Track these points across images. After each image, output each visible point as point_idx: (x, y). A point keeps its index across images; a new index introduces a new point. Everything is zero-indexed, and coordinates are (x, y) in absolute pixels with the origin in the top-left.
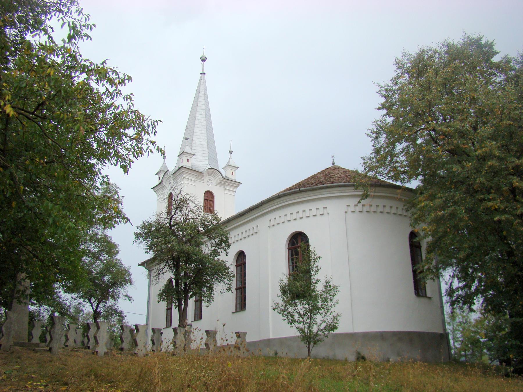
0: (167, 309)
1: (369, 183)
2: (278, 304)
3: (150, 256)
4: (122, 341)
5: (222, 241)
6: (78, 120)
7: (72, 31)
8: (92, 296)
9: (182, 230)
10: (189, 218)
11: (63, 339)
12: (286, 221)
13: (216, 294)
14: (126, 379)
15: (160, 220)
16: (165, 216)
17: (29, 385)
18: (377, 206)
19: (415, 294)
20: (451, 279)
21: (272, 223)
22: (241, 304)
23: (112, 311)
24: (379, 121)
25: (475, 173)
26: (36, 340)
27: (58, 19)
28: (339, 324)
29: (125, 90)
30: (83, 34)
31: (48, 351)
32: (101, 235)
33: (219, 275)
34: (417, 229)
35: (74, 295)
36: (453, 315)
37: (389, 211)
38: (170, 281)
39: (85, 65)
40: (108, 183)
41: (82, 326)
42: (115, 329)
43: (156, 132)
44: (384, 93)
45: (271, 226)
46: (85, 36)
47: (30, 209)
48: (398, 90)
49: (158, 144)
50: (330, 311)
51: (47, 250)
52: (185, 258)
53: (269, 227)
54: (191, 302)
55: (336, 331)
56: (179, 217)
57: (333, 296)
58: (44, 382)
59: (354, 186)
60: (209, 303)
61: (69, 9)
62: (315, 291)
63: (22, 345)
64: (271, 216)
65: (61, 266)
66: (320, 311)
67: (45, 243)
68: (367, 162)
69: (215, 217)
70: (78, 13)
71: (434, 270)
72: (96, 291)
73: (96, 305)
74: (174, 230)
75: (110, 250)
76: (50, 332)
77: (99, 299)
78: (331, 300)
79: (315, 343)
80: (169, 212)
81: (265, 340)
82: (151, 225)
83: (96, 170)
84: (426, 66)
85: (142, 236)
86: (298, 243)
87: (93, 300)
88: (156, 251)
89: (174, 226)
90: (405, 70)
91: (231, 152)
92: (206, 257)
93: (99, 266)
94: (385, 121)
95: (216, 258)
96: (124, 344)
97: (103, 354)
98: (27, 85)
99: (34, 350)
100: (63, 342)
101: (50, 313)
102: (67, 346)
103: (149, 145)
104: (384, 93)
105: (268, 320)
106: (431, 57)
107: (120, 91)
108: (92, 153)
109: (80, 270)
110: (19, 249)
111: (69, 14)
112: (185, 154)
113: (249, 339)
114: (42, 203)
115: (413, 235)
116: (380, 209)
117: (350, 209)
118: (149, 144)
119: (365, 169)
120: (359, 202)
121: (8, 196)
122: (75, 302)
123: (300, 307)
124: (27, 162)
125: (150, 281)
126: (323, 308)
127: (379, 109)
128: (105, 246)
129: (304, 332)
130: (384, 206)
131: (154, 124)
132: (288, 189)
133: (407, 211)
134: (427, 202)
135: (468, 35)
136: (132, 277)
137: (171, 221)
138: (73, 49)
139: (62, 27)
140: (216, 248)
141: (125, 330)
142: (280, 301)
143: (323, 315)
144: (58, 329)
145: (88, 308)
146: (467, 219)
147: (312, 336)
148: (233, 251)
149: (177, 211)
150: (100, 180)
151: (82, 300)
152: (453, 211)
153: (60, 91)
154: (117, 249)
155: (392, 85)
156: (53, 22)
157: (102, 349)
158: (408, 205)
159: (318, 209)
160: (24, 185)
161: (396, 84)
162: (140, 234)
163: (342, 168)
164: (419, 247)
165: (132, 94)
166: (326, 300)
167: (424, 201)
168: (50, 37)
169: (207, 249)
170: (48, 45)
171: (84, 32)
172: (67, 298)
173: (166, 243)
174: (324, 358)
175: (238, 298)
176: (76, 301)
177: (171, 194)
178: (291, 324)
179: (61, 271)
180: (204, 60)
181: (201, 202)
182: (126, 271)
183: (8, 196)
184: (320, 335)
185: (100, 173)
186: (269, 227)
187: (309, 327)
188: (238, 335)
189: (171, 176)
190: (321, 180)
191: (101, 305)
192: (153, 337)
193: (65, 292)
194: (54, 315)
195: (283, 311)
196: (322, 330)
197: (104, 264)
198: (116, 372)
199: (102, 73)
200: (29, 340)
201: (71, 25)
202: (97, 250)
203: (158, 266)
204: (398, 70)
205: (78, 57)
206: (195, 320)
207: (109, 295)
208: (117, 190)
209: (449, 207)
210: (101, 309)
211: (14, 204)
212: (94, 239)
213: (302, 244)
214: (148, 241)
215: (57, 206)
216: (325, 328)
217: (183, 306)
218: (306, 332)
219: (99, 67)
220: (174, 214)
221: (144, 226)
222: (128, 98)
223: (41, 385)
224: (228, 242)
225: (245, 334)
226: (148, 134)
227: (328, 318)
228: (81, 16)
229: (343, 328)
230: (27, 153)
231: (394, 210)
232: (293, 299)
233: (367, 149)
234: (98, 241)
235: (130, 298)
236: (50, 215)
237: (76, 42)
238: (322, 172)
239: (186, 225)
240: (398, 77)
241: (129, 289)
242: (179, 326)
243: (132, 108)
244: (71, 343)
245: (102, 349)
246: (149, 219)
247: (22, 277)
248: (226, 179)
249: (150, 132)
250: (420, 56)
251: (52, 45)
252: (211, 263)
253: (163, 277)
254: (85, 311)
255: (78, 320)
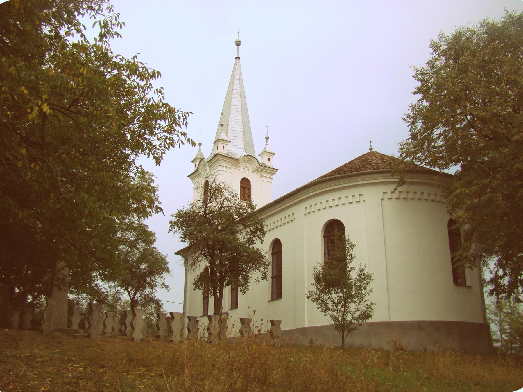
0: (204, 298)
1: (406, 169)
2: (312, 292)
3: (186, 244)
4: (159, 329)
5: (257, 229)
6: (110, 116)
7: (103, 30)
8: (128, 285)
9: (217, 219)
10: (224, 206)
11: (101, 326)
12: (311, 212)
13: (252, 282)
14: (160, 363)
15: (195, 208)
16: (200, 204)
17: (69, 366)
18: (415, 193)
19: (454, 282)
20: (496, 267)
21: (308, 211)
22: (277, 293)
23: (149, 300)
24: (415, 105)
25: (513, 159)
26: (75, 327)
27: (90, 17)
28: (373, 313)
29: (156, 83)
30: (113, 33)
31: (86, 337)
32: (137, 224)
33: (254, 264)
34: (455, 216)
35: (112, 284)
36: (499, 305)
37: (427, 198)
38: (206, 269)
39: (116, 62)
40: (143, 172)
41: (120, 314)
42: (153, 318)
43: (187, 123)
44: (420, 76)
45: (307, 214)
46: (115, 35)
47: (67, 201)
48: (434, 73)
49: (188, 136)
50: (364, 300)
51: (84, 239)
52: (220, 246)
53: (305, 215)
54: (227, 291)
55: (370, 320)
56: (213, 205)
57: (367, 284)
58: (83, 365)
59: (390, 172)
60: (244, 291)
61: (100, 7)
62: (349, 280)
63: (62, 331)
64: (307, 204)
65: (98, 255)
66: (354, 300)
67: (83, 232)
68: (404, 148)
69: (250, 206)
70: (109, 10)
71: (472, 259)
72: (133, 279)
73: (133, 294)
74: (209, 219)
75: (146, 238)
76: (88, 319)
77: (136, 288)
78: (365, 288)
79: (349, 332)
80: (205, 201)
81: (300, 329)
82: (186, 213)
83: (131, 160)
84: (462, 47)
85: (177, 225)
86: (334, 232)
87: (130, 288)
88: (192, 239)
89: (209, 214)
90: (442, 52)
91: (267, 138)
92: (242, 245)
93: (136, 254)
94: (422, 105)
95: (251, 246)
96: (160, 331)
97: (139, 340)
98: (62, 83)
99: (73, 336)
100: (102, 330)
101: (89, 301)
102: (105, 333)
103: (180, 136)
104: (420, 76)
105: (304, 311)
106: (469, 39)
107: (151, 84)
108: (126, 145)
109: (116, 258)
110: (58, 239)
111: (100, 12)
112: (221, 142)
113: (284, 327)
114: (78, 194)
115: (451, 222)
116: (418, 196)
117: (387, 196)
118: (180, 135)
119: (401, 155)
120: (396, 189)
121: (46, 188)
122: (113, 291)
123: (334, 295)
124: (64, 155)
125: (187, 270)
126: (357, 297)
127: (415, 93)
128: (142, 235)
129: (338, 320)
130: (422, 193)
131: (185, 115)
132: (324, 176)
133: (446, 197)
134: (463, 189)
135: (510, 13)
136: (168, 265)
137: (205, 210)
138: (104, 46)
139: (93, 27)
140: (251, 236)
141: (161, 318)
142: (314, 289)
143: (357, 304)
144: (96, 316)
145: (125, 297)
146: (504, 206)
147: (346, 324)
148: (269, 239)
149: (212, 200)
150: (134, 171)
151: (119, 288)
152: (489, 197)
153: (93, 89)
154: (154, 238)
155: (428, 69)
156: (85, 19)
157: (138, 335)
158: (447, 191)
159: (354, 196)
160: (61, 176)
161: (433, 67)
162: (175, 223)
163: (380, 154)
164: (460, 235)
165: (162, 88)
166: (360, 288)
167: (460, 187)
168: (82, 35)
169: (242, 237)
170: (81, 43)
171: (114, 30)
172: (105, 286)
173: (201, 232)
174: (359, 347)
175: (274, 287)
176: (113, 290)
177: (207, 182)
178: (325, 312)
179: (98, 260)
180: (238, 44)
181: (237, 190)
182: (163, 259)
183: (46, 188)
184: (354, 323)
185: (134, 164)
186: (305, 215)
187: (343, 315)
188: (272, 322)
189: (207, 163)
190: (358, 166)
191: (138, 294)
192: (189, 324)
193: (103, 281)
194: (92, 302)
195: (318, 299)
196: (356, 318)
197: (140, 252)
198: (151, 357)
199: (133, 68)
200: (69, 327)
201: (102, 24)
202: (134, 238)
203: (193, 255)
204: (434, 53)
205: (110, 54)
206: (232, 308)
207: (147, 283)
208: (153, 178)
209: (485, 194)
210: (138, 297)
211: (52, 195)
212: (130, 227)
213: (336, 231)
214: (183, 230)
215: (93, 198)
216: (359, 316)
217: (218, 294)
218: (340, 320)
219: (130, 62)
220: (209, 203)
221: (179, 215)
222: (159, 91)
223: (81, 367)
224: (263, 230)
225: (280, 322)
226: (179, 125)
227: (363, 306)
228: (112, 13)
229: (377, 317)
230: (63, 147)
231: (432, 197)
232: (326, 288)
233: (404, 134)
234: (135, 229)
235: (166, 287)
236: (85, 207)
237: (107, 40)
238: (360, 158)
239: (223, 214)
240: (435, 60)
241: (166, 278)
242: (215, 314)
243: (163, 101)
244: (109, 330)
245: (138, 335)
246: (184, 207)
247: (61, 266)
248: (263, 166)
249: (181, 124)
250: (457, 37)
251: (85, 43)
252: (246, 252)
253: (198, 266)
254: (123, 300)
255: (116, 308)
